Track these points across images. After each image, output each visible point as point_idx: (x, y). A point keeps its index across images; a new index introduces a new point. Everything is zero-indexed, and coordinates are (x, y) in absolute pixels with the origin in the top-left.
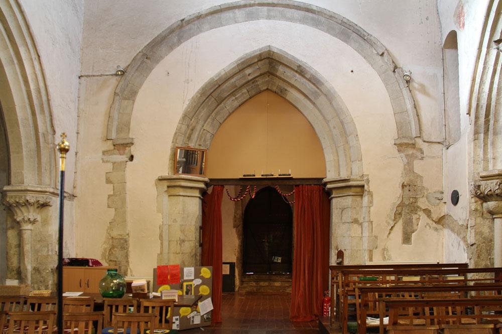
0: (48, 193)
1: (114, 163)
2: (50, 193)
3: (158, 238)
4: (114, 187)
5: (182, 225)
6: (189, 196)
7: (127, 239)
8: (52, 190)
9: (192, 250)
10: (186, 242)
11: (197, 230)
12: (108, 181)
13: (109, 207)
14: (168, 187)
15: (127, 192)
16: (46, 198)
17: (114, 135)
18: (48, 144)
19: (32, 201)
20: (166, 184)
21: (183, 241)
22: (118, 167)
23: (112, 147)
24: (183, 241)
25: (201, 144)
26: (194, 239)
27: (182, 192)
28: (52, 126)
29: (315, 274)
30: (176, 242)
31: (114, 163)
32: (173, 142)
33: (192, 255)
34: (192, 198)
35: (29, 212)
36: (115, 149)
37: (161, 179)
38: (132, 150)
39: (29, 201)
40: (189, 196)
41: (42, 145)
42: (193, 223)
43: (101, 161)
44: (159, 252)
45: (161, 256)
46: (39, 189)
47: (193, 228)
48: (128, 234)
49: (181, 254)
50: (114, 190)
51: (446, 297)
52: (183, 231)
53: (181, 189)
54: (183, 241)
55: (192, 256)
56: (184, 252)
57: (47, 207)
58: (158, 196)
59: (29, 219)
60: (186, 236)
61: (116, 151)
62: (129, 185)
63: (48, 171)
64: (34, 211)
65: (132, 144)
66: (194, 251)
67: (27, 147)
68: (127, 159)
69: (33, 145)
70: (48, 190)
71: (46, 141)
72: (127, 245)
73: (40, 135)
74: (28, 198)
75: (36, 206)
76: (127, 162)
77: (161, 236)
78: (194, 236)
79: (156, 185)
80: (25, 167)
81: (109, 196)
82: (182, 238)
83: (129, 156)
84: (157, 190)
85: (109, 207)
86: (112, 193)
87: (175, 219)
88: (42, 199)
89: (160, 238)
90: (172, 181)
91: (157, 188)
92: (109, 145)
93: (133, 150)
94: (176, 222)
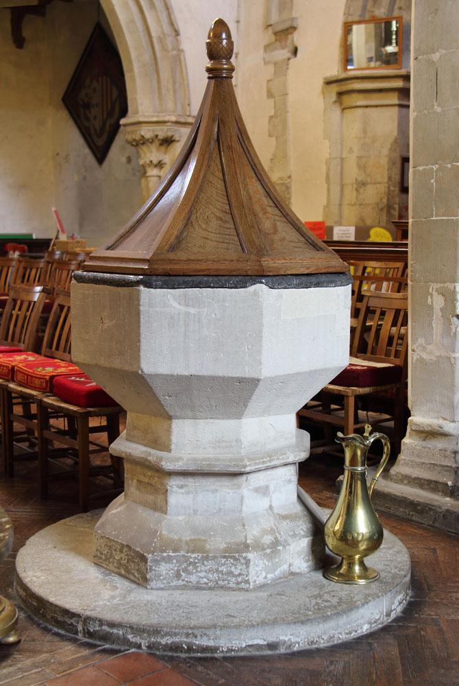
0: (169, 124)
1: (275, 64)
2: (172, 122)
3: (325, 182)
4: (275, 103)
5: (362, 157)
6: (376, 106)
7: (289, 185)
8: (173, 119)
9: (381, 199)
10: (369, 186)
11: (394, 164)
12: (270, 95)
13: (270, 136)
14: (340, 94)
15: (290, 109)
16: (167, 131)
17: (274, 18)
18: (167, 51)
19: (148, 135)
20: (335, 88)
21: (364, 184)
22: (281, 68)
23: (273, 38)
24: (363, 184)
25: (403, 6)
26: (386, 180)
27: (360, 100)
28: (172, 24)
29: (123, 265)
30: (350, 187)
31: (275, 64)
32: (345, 14)
33: (380, 207)
34: (384, 109)
35: (151, 152)
36: (276, 40)
37: (329, 83)
38: (295, 39)
39: (145, 136)
40: (376, 106)
41: (159, 54)
42: (385, 152)
43: (263, 63)
44: (325, 204)
45: (327, 209)
46: (155, 119)
47: (384, 161)
48: (290, 177)
49: (358, 206)
50: (275, 107)
51: (6, 318)
52: (362, 167)
53: (361, 96)
54: (364, 184)
55: (381, 210)
56: (364, 202)
57: (174, 143)
58: (325, 110)
59: (151, 161)
60: (369, 175)
61: (278, 44)
62: (291, 98)
63: (171, 92)
64: (158, 150)
65: (294, 28)
66: (385, 201)
67: (139, 62)
68: (289, 55)
69: (147, 57)
70: (167, 118)
71: (164, 49)
72: (288, 193)
73: (155, 41)
74: (143, 133)
75: (157, 142)
76: (289, 59)
77: (328, 177)
78: (386, 176)
79: (323, 93)
80: (139, 90)
81: (271, 117)
82: (360, 179)
83: (291, 48)
84: (324, 102)
85: (270, 136)
86: (272, 113)
87: (351, 148)
88: (162, 132)
89: (326, 181)
90: (343, 83)
91: (324, 98)
92: (269, 37)
93: (297, 38)
94: (353, 151)
